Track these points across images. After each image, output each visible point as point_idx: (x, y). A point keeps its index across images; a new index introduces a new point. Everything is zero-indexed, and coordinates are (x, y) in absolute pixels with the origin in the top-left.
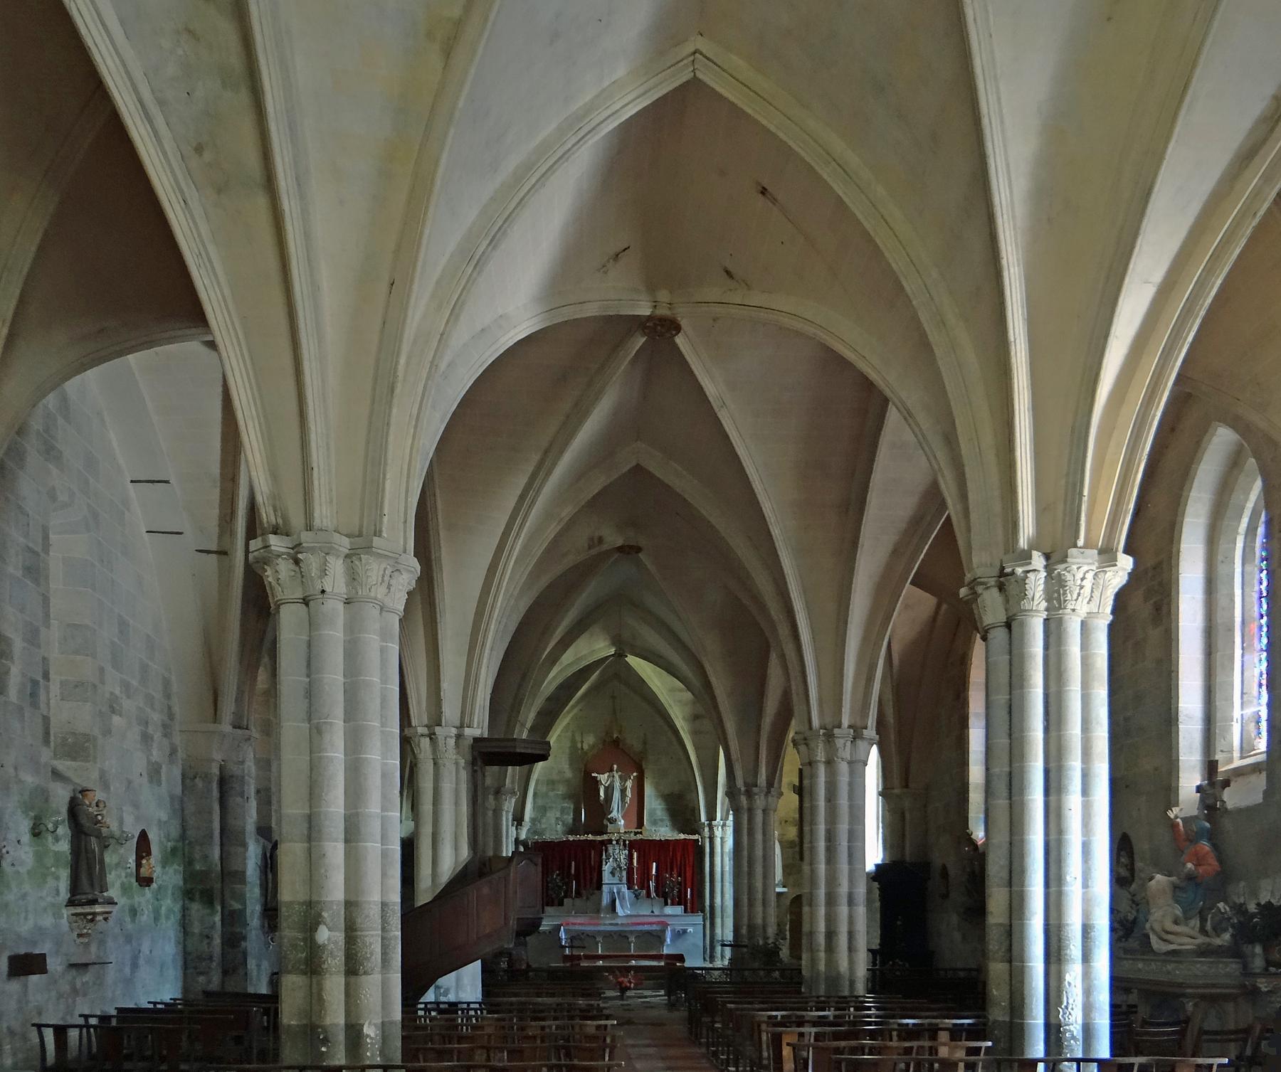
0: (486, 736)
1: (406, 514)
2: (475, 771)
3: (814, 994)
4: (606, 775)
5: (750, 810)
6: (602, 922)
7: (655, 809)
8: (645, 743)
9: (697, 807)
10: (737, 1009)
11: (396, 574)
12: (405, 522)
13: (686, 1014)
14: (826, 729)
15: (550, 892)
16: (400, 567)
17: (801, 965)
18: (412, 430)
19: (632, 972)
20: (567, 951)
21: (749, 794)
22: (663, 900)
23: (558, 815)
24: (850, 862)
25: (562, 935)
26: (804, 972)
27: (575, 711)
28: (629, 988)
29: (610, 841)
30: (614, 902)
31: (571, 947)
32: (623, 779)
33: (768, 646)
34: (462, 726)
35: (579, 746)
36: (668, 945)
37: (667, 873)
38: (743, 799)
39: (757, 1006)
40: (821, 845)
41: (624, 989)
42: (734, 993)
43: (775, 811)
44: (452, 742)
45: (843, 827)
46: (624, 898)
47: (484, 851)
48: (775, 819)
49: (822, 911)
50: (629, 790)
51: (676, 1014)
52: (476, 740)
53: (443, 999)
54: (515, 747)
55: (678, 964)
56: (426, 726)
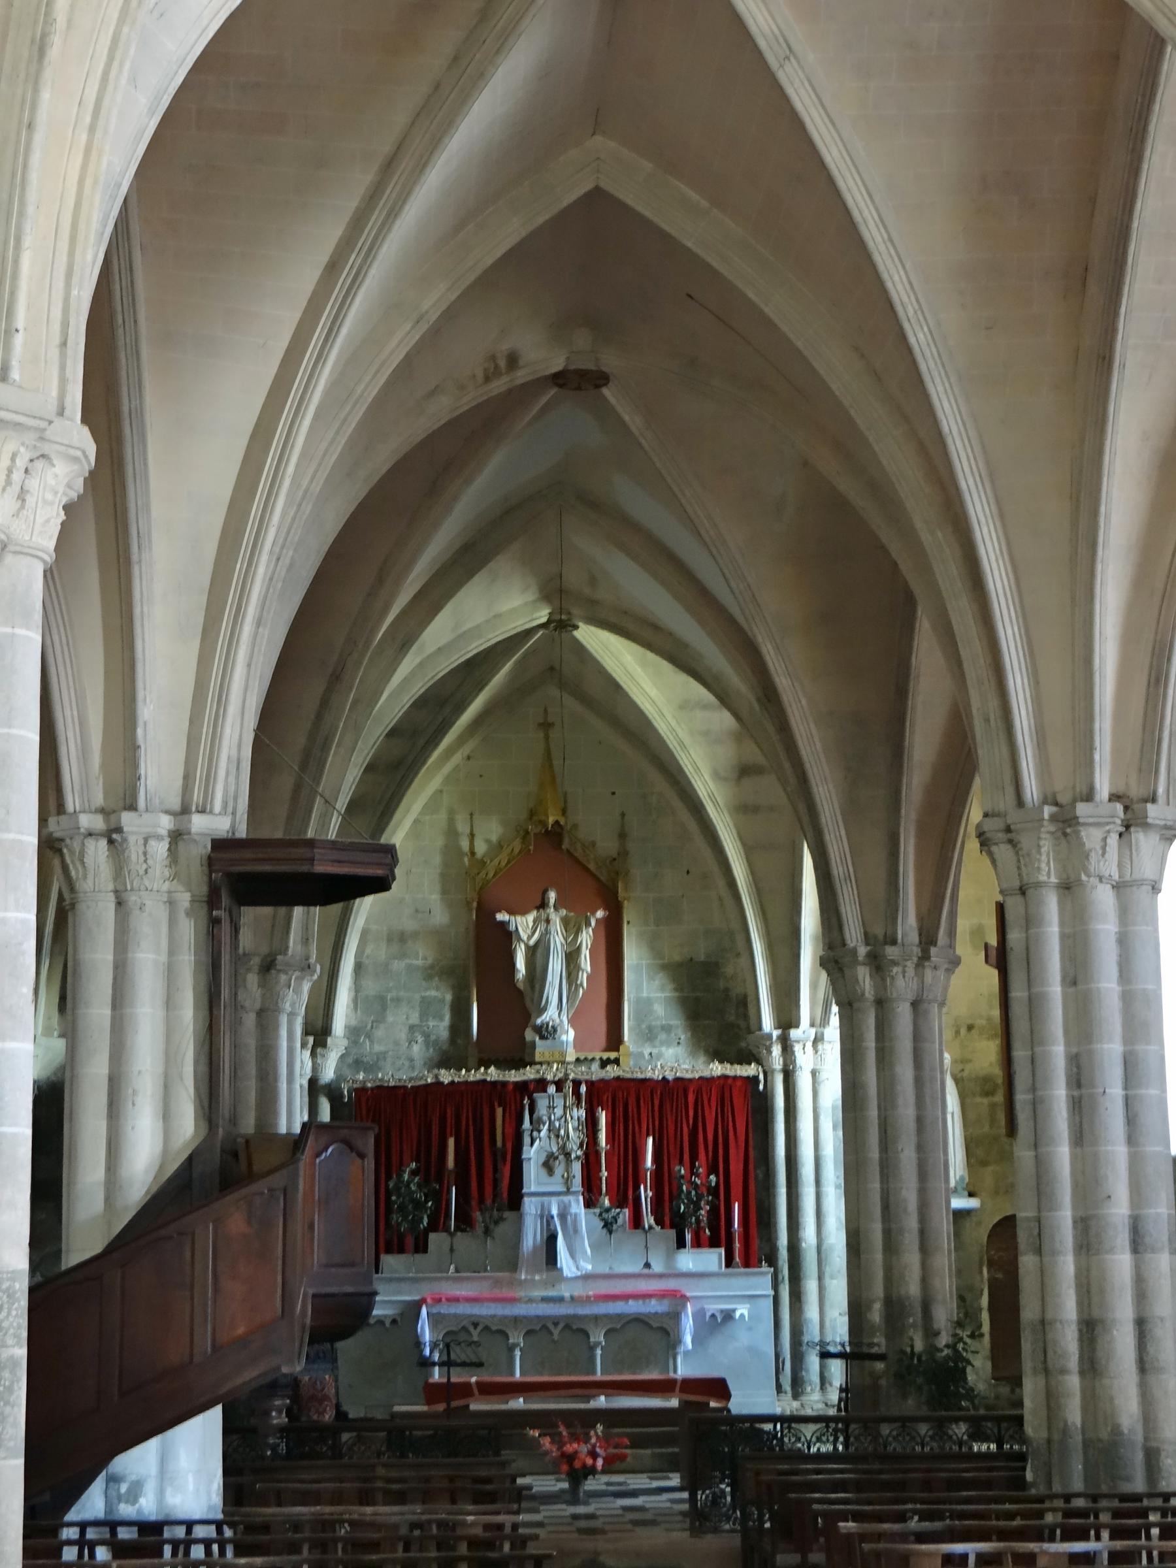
0: (242, 833)
1: (65, 324)
2: (215, 922)
3: (1057, 1488)
4: (531, 917)
5: (881, 1003)
6: (521, 1293)
7: (649, 1001)
8: (623, 836)
9: (750, 992)
10: (863, 1537)
11: (39, 464)
12: (64, 344)
13: (736, 1541)
14: (1056, 804)
15: (395, 1218)
16: (47, 448)
17: (1020, 1404)
18: (84, 137)
19: (600, 1428)
20: (436, 1375)
21: (877, 963)
22: (672, 1233)
23: (415, 1019)
24: (1132, 1139)
25: (426, 1332)
26: (1029, 1430)
27: (457, 758)
28: (592, 1471)
29: (542, 1084)
30: (551, 1239)
31: (447, 1364)
32: (572, 928)
33: (910, 601)
34: (185, 810)
35: (465, 844)
36: (686, 1353)
37: (681, 1163)
38: (864, 977)
39: (914, 1524)
40: (1059, 1093)
41: (578, 1475)
42: (858, 1487)
43: (942, 1004)
44: (160, 849)
45: (1111, 1049)
46: (576, 1231)
47: (234, 1120)
48: (941, 1022)
49: (1067, 1266)
50: (585, 953)
51: (709, 1542)
52: (220, 845)
53: (126, 1511)
54: (312, 860)
55: (713, 1404)
56: (102, 811)
